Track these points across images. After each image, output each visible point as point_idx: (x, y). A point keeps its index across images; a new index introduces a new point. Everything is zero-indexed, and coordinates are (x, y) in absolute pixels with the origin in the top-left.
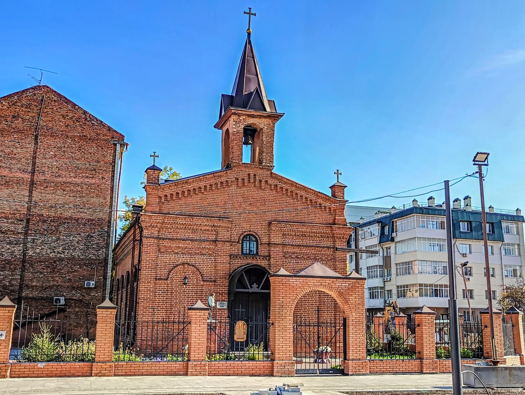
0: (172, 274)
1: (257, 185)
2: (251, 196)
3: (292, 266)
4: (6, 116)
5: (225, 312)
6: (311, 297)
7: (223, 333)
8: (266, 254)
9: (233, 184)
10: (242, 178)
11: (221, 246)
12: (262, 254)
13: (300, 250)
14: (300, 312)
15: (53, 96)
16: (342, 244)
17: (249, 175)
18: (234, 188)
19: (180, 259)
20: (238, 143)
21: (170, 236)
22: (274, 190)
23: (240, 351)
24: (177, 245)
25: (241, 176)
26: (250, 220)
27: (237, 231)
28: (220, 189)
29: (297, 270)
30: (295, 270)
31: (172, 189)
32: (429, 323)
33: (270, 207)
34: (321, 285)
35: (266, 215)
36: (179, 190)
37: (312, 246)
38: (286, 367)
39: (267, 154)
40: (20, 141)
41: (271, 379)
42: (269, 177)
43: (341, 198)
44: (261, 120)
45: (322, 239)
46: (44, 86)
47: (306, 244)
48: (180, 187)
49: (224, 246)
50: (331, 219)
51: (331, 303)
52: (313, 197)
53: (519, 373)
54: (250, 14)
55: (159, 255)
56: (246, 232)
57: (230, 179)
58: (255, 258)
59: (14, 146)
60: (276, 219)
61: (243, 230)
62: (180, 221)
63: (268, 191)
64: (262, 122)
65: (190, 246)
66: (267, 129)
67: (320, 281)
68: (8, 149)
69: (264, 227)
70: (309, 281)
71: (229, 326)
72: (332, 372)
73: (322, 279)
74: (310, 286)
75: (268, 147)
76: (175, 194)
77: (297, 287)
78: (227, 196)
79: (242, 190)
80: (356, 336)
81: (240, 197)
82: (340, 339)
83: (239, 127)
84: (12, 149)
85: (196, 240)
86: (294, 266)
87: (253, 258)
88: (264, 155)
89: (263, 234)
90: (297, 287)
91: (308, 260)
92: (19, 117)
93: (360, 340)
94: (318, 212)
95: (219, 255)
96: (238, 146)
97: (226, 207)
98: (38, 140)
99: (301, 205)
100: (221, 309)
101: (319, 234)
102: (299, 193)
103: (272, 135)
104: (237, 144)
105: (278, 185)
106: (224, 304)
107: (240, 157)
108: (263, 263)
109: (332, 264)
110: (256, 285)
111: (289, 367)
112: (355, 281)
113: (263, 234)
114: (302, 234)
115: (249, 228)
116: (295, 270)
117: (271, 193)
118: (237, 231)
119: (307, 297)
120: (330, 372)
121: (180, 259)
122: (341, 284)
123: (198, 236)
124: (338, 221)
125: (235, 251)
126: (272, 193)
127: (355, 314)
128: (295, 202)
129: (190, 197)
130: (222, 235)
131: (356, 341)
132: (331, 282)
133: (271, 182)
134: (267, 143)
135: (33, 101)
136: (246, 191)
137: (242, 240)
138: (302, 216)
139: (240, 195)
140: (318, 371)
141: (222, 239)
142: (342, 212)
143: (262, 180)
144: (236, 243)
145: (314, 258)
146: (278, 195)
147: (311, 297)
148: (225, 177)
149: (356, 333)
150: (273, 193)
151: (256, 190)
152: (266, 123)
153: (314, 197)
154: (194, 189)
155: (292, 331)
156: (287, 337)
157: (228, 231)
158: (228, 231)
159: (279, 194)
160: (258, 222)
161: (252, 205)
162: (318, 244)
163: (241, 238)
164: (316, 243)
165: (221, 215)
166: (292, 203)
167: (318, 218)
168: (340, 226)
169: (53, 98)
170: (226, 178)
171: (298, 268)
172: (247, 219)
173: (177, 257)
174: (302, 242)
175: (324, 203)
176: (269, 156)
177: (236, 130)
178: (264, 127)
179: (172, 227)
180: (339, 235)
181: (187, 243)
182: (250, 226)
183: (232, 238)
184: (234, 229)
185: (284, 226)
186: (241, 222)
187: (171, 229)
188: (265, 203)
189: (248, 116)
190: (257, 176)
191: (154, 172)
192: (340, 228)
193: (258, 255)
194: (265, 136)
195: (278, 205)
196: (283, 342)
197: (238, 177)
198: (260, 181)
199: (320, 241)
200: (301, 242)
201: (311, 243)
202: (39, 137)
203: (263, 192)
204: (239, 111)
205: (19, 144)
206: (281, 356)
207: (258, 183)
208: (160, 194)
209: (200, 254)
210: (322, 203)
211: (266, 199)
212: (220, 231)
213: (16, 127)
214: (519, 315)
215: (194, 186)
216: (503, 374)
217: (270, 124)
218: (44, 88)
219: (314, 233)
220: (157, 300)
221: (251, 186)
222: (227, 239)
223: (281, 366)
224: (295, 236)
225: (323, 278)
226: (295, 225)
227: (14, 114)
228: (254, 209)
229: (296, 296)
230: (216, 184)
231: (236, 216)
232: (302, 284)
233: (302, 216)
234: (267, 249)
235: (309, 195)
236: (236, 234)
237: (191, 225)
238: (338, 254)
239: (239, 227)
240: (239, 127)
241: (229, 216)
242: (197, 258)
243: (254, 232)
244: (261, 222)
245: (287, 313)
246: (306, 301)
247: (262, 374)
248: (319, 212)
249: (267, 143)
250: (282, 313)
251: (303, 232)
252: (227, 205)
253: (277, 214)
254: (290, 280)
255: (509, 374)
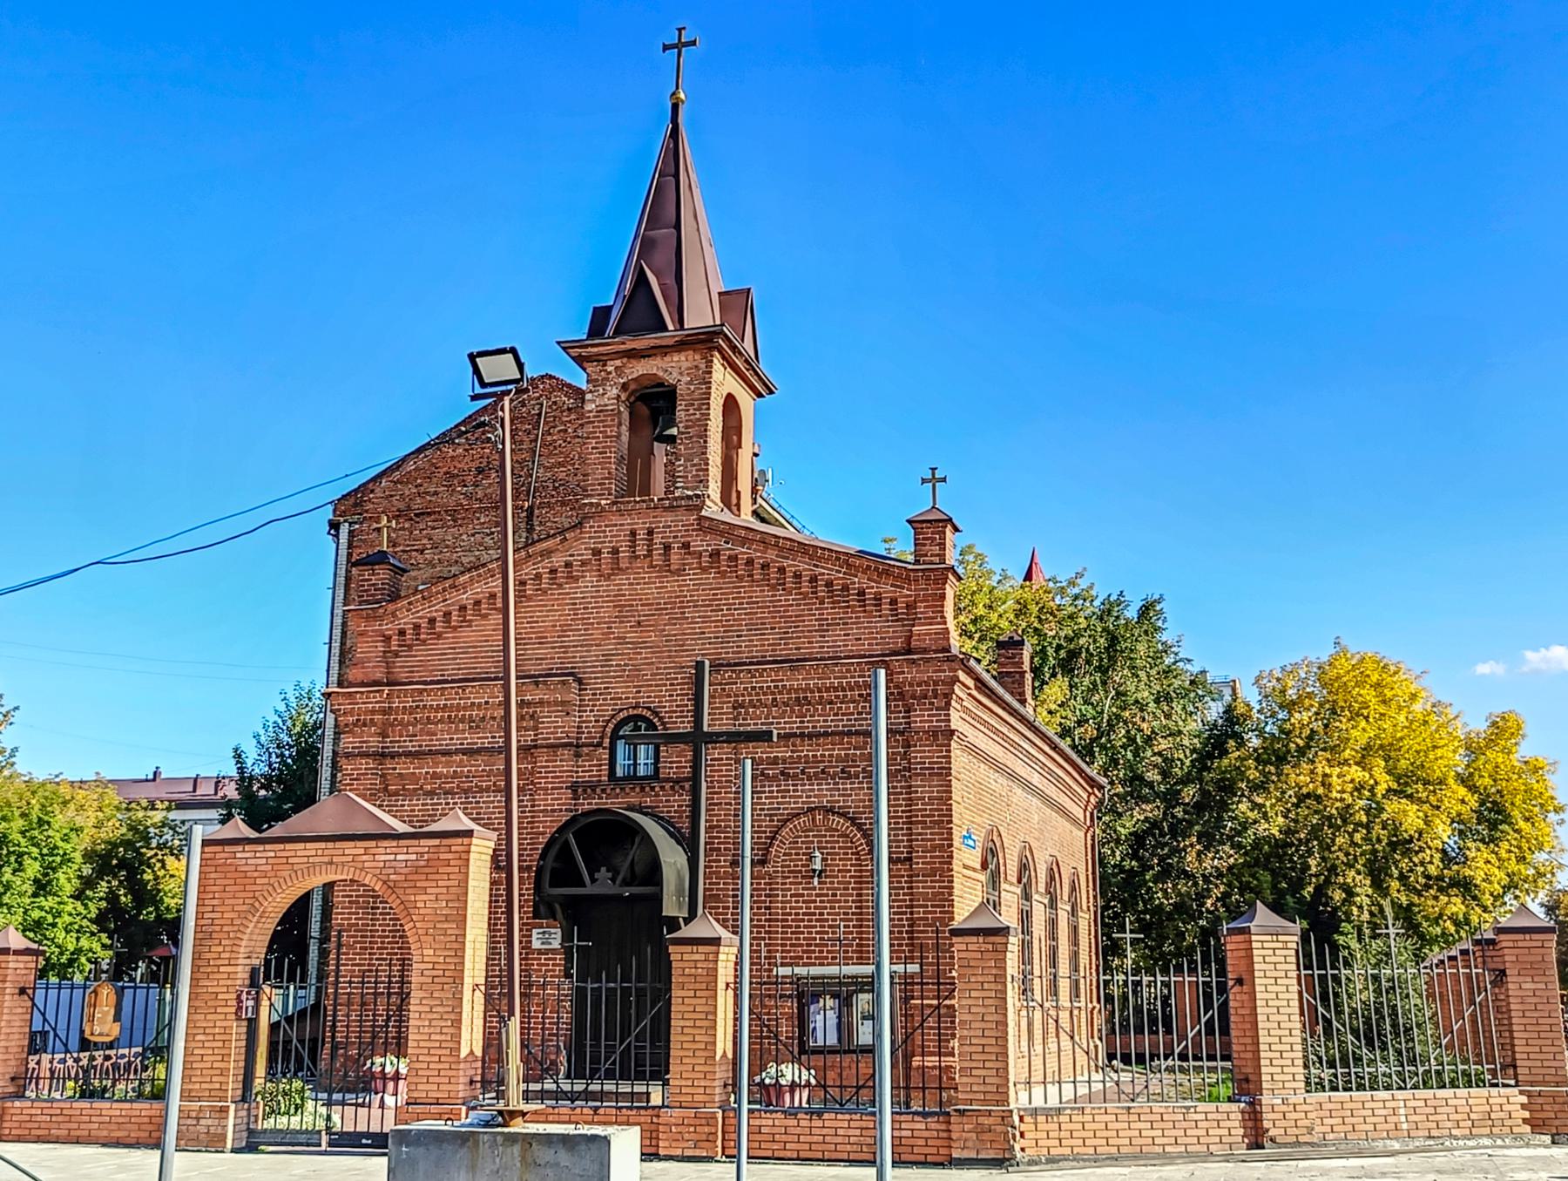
0: (776, 851)
1: (657, 560)
2: (641, 600)
3: (765, 804)
4: (464, 471)
5: (555, 959)
6: (829, 901)
7: (550, 1023)
8: (684, 773)
9: (586, 571)
10: (613, 548)
11: (546, 761)
12: (674, 773)
13: (792, 751)
14: (794, 952)
15: (564, 398)
16: (933, 715)
17: (633, 533)
18: (589, 582)
19: (438, 810)
20: (601, 442)
21: (413, 746)
22: (712, 568)
23: (605, 1079)
24: (431, 771)
25: (610, 542)
26: (636, 675)
27: (598, 711)
28: (550, 589)
29: (783, 814)
30: (776, 815)
31: (418, 612)
32: (695, 976)
33: (698, 623)
34: (331, 863)
35: (687, 650)
36: (436, 611)
37: (834, 734)
38: (202, 1122)
39: (689, 461)
40: (493, 530)
41: (55, 1153)
42: (693, 530)
43: (937, 559)
44: (667, 358)
45: (865, 707)
46: (542, 377)
47: (813, 727)
48: (439, 603)
49: (556, 761)
50: (901, 637)
51: (899, 920)
52: (837, 571)
53: (564, 1157)
54: (680, 45)
55: (385, 803)
56: (623, 709)
57: (578, 555)
58: (647, 789)
59: (481, 544)
60: (719, 659)
61: (617, 704)
62: (432, 700)
63: (694, 574)
64: (673, 364)
65: (466, 769)
66: (690, 383)
67: (326, 852)
68: (469, 554)
69: (681, 689)
70: (293, 853)
71: (571, 1001)
72: (370, 1142)
73: (330, 845)
74: (295, 867)
75: (691, 437)
76: (424, 623)
77: (256, 874)
78: (569, 610)
79: (614, 585)
80: (430, 1026)
81: (608, 607)
82: (923, 1039)
83: (603, 394)
84: (477, 553)
85: (479, 751)
86: (773, 803)
87: (643, 789)
88: (680, 466)
89: (676, 712)
90: (256, 874)
91: (822, 779)
92: (490, 469)
93: (443, 1037)
94: (856, 618)
95: (540, 789)
96: (600, 453)
97: (569, 641)
98: (535, 519)
99: (800, 605)
100: (547, 952)
101: (852, 689)
102: (789, 566)
103: (705, 399)
104: (597, 448)
105: (723, 550)
106: (553, 936)
107: (605, 484)
108: (674, 801)
109: (901, 787)
110: (599, 871)
111: (209, 1122)
112: (436, 842)
113: (676, 712)
114: (798, 699)
115: (633, 698)
116: (776, 815)
117: (701, 579)
118: (598, 711)
119: (815, 901)
120: (364, 1141)
121: (438, 810)
122: (392, 857)
123: (487, 738)
124: (918, 640)
125: (592, 771)
126: (706, 579)
127: (431, 952)
128: (780, 595)
129: (467, 626)
130: (550, 728)
131: (430, 1040)
132: (362, 851)
133: (699, 546)
134: (686, 427)
135: (521, 422)
136: (624, 584)
137: (611, 738)
138: (800, 637)
139: (607, 602)
140: (325, 1139)
141: (550, 738)
142: (937, 606)
143: (671, 543)
144: (592, 748)
145: (843, 771)
146: (724, 583)
147: (829, 901)
148: (562, 552)
149: (430, 1016)
150: (709, 578)
151: (656, 577)
152: (685, 365)
153: (840, 572)
154: (477, 603)
155: (233, 1010)
156: (217, 1030)
157: (568, 714)
158: (568, 714)
159: (729, 577)
160: (662, 674)
161: (643, 626)
162: (854, 726)
163: (609, 730)
164: (848, 720)
165: (552, 669)
166: (770, 601)
167: (857, 639)
168: (915, 657)
169: (564, 403)
170: (566, 556)
171: (787, 809)
172: (629, 670)
173: (432, 805)
174: (800, 722)
175: (873, 587)
176: (695, 465)
177: (593, 406)
178: (679, 381)
179: (415, 718)
180: (919, 685)
181: (455, 761)
182: (637, 692)
183: (583, 733)
184: (588, 705)
185: (730, 677)
186: (611, 683)
187: (414, 725)
188: (684, 613)
189: (629, 357)
190: (659, 533)
191: (373, 570)
192: (914, 662)
193: (658, 778)
194: (683, 407)
195: (722, 615)
196: (206, 1045)
197: (600, 546)
198: (667, 548)
199: (862, 713)
200: (796, 722)
201: (831, 722)
202: (536, 512)
203: (678, 581)
204: (589, 349)
205: (493, 539)
206: (197, 1086)
207: (660, 554)
208: (388, 627)
209: (493, 791)
210: (867, 588)
211: (688, 602)
212: (546, 717)
213: (486, 495)
214: (1254, 938)
215: (478, 593)
216: (498, 1160)
217: (696, 367)
218: (543, 383)
219: (836, 689)
220: (378, 931)
221: (639, 568)
222: (564, 738)
223: (188, 1117)
224: (776, 706)
225: (334, 841)
226: (765, 670)
227: (481, 463)
228: (651, 637)
229: (251, 901)
230: (538, 577)
231: (597, 667)
232: (272, 864)
233: (800, 637)
234: (686, 756)
235: (823, 567)
236: (596, 721)
237: (465, 709)
238: (919, 752)
239: (603, 700)
240: (603, 394)
241: (575, 668)
242: (483, 802)
243: (649, 708)
244: (670, 674)
245: (223, 955)
246: (814, 914)
247: (144, 1141)
248: (860, 617)
249: (686, 427)
250: (208, 955)
251: (796, 691)
252: (569, 636)
253: (722, 643)
254: (238, 855)
255: (523, 1158)
